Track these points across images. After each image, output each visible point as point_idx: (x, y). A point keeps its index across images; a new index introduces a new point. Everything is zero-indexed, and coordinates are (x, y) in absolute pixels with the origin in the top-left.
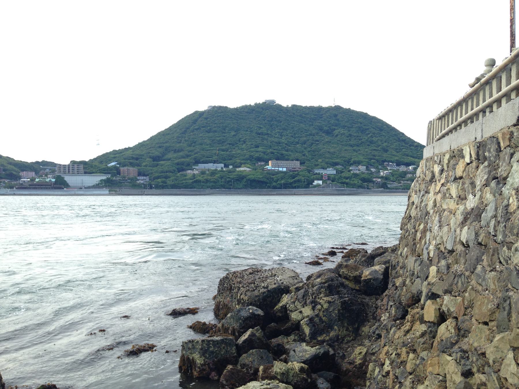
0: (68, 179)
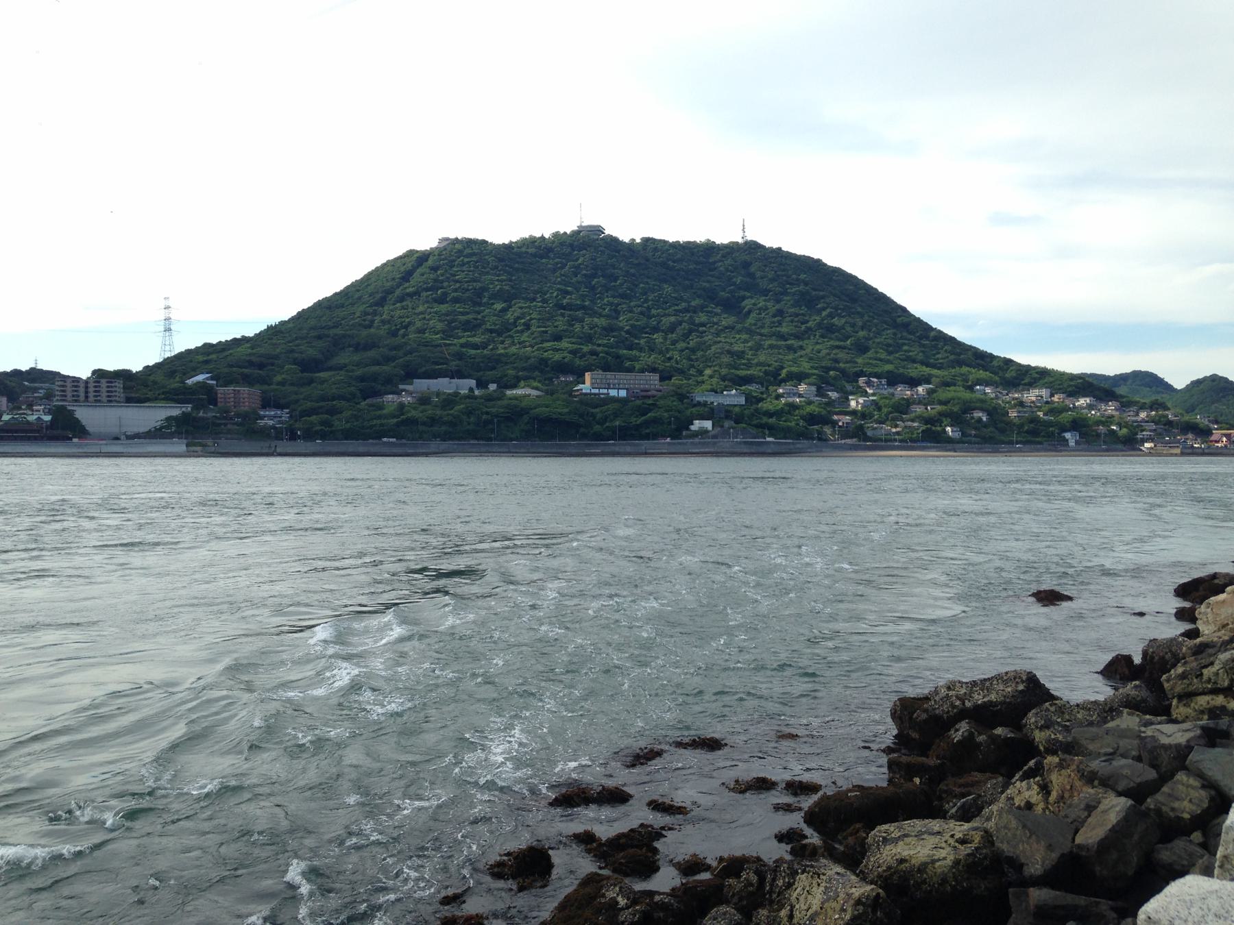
0: (84, 414)
